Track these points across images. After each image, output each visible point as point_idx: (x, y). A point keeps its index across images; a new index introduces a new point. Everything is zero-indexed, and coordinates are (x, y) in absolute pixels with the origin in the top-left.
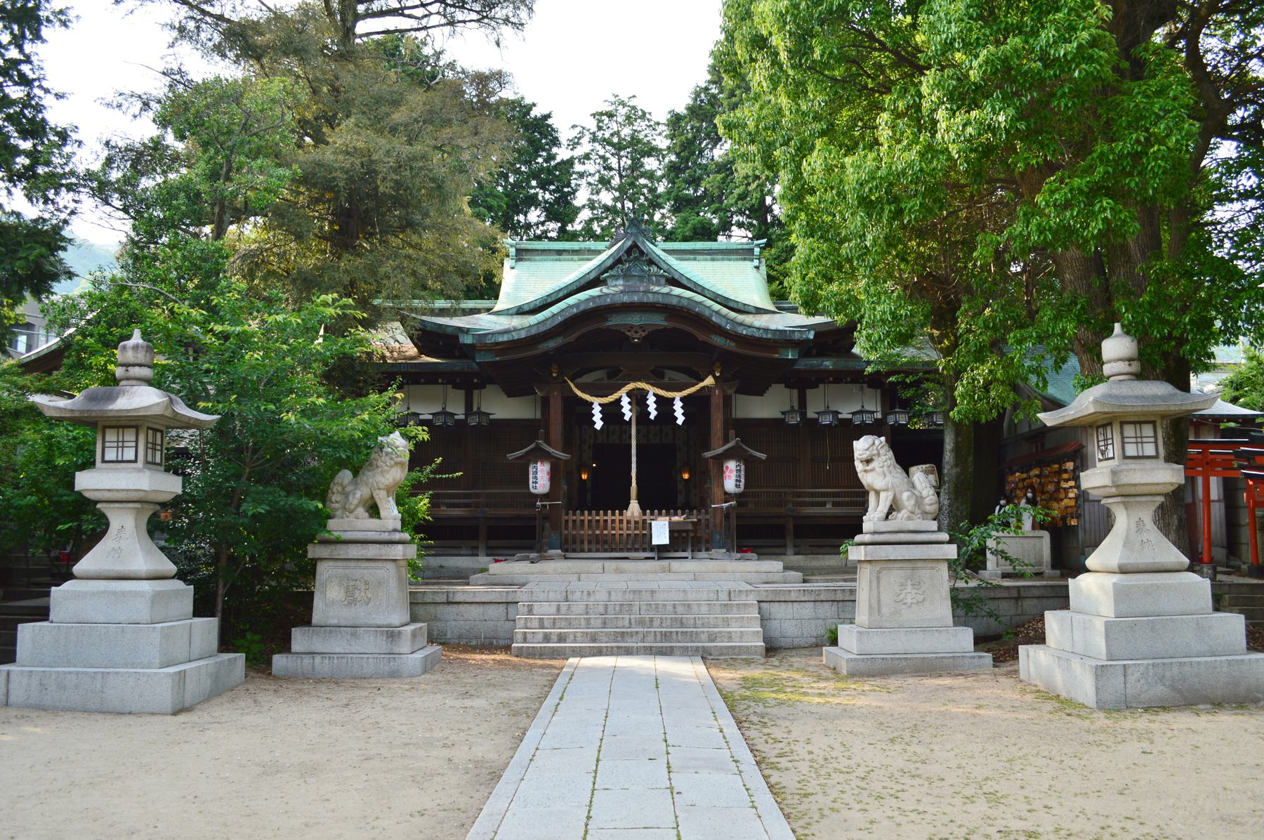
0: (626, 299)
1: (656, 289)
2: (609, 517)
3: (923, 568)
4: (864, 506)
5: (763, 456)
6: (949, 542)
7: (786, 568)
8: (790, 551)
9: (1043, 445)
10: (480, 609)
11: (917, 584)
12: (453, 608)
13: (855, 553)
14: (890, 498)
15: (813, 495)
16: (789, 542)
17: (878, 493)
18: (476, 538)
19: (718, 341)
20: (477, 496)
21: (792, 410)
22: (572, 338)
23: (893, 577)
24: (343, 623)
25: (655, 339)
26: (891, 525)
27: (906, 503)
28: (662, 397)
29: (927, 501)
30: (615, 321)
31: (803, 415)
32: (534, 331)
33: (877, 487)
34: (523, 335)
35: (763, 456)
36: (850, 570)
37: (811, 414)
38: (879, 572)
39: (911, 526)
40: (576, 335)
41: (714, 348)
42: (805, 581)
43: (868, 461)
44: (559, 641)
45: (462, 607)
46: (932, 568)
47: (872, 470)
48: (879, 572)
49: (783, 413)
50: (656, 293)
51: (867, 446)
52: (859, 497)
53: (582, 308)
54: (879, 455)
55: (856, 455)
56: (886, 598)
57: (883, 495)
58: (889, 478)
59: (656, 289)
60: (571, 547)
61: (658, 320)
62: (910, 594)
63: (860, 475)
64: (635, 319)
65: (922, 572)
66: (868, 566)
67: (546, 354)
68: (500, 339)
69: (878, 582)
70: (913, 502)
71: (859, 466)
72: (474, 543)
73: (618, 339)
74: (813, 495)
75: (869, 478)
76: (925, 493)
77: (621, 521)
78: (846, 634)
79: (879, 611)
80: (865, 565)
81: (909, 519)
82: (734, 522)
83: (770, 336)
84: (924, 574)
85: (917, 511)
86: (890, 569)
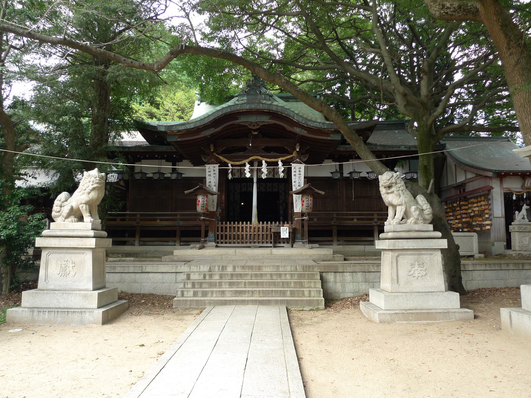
0: (248, 107)
1: (264, 102)
2: (240, 225)
3: (425, 254)
4: (385, 217)
5: (323, 193)
6: (442, 238)
7: (334, 253)
8: (335, 243)
9: (464, 190)
10: (160, 276)
11: (421, 264)
12: (143, 275)
13: (379, 245)
14: (404, 210)
15: (347, 215)
16: (335, 238)
17: (394, 207)
18: (175, 236)
19: (297, 130)
20: (176, 215)
21: (336, 172)
22: (219, 129)
23: (406, 261)
24: (57, 288)
25: (265, 131)
26: (404, 227)
27: (414, 213)
28: (269, 162)
29: (426, 212)
30: (242, 120)
31: (342, 173)
32: (198, 124)
33: (395, 202)
34: (192, 126)
35: (323, 193)
36: (378, 254)
37: (346, 174)
38: (397, 257)
39: (417, 227)
40: (221, 127)
41: (296, 134)
42: (345, 260)
43: (390, 187)
44: (202, 296)
45: (151, 275)
46: (431, 254)
47: (393, 192)
48: (397, 257)
49: (332, 173)
50: (265, 103)
51: (389, 178)
52: (382, 211)
53: (224, 112)
54: (396, 184)
55: (381, 184)
56: (403, 273)
57: (398, 209)
58: (402, 197)
59: (264, 102)
60: (221, 240)
61: (266, 120)
62: (417, 271)
63: (383, 196)
64: (253, 119)
65: (425, 257)
66: (390, 253)
67: (205, 138)
68: (180, 129)
69: (397, 263)
70: (417, 213)
71: (383, 191)
72: (174, 239)
73: (244, 132)
74: (347, 215)
75: (389, 197)
76: (424, 207)
77: (250, 227)
78: (375, 297)
79: (398, 282)
80: (387, 252)
81: (416, 223)
82: (306, 228)
83: (325, 127)
84: (426, 257)
85: (420, 218)
86: (405, 254)
